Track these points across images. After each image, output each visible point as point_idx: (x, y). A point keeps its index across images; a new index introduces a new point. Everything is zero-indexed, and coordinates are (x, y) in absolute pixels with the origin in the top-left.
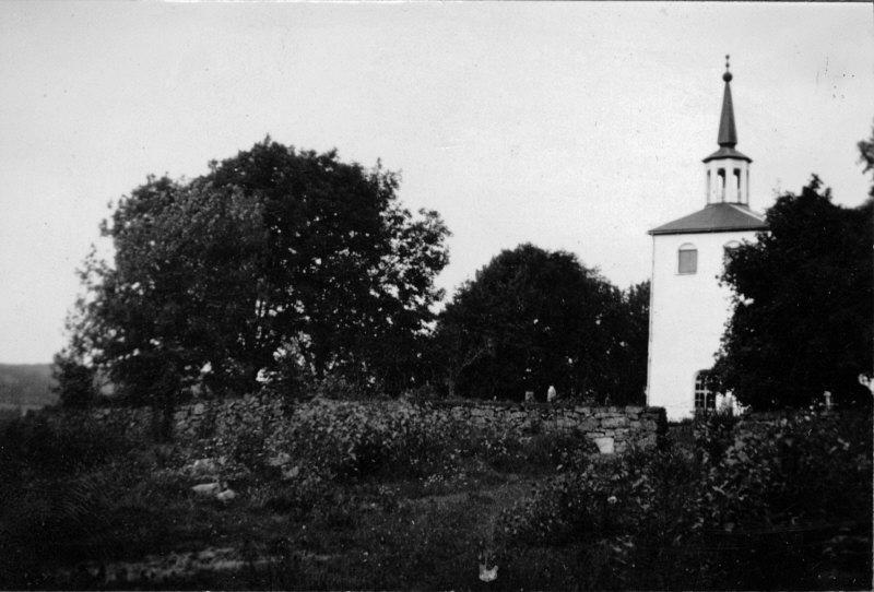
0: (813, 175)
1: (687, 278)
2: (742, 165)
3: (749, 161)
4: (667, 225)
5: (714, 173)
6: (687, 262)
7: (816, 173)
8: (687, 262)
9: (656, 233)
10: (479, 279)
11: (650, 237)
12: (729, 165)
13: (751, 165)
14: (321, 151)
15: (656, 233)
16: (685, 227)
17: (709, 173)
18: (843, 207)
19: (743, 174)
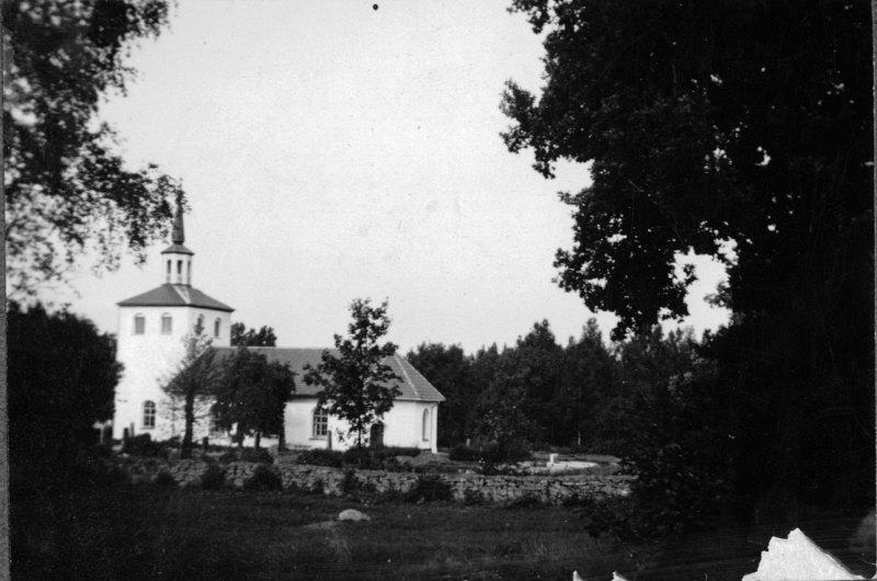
0: (546, 173)
1: (139, 337)
2: (184, 258)
3: (191, 254)
4: (132, 299)
5: (174, 266)
6: (140, 324)
7: (549, 180)
8: (140, 324)
9: (123, 304)
10: (55, 318)
11: (118, 307)
12: (174, 258)
13: (193, 257)
14: (574, 222)
15: (123, 304)
16: (140, 301)
17: (169, 262)
18: (470, 350)
19: (184, 266)
